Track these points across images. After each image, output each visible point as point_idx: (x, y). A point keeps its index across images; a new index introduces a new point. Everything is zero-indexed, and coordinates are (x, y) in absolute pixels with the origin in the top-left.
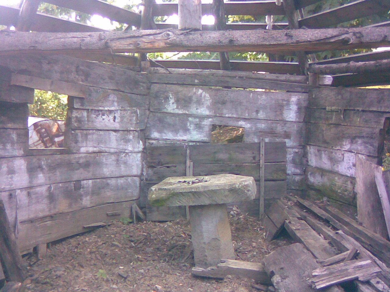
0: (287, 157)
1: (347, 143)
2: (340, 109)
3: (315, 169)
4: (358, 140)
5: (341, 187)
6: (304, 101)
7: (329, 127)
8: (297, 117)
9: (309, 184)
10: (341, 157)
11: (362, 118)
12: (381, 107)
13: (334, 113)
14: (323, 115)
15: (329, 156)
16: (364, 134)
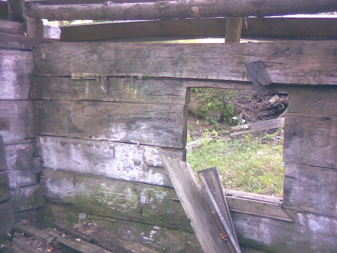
0: (6, 162)
1: (119, 129)
2: (99, 77)
3: (60, 174)
4: (141, 124)
5: (114, 197)
6: (27, 64)
7: (80, 106)
8: (16, 91)
9: (49, 195)
10: (110, 152)
11: (142, 89)
12: (181, 72)
13: (87, 83)
14: (65, 86)
15: (85, 152)
16: (152, 115)
